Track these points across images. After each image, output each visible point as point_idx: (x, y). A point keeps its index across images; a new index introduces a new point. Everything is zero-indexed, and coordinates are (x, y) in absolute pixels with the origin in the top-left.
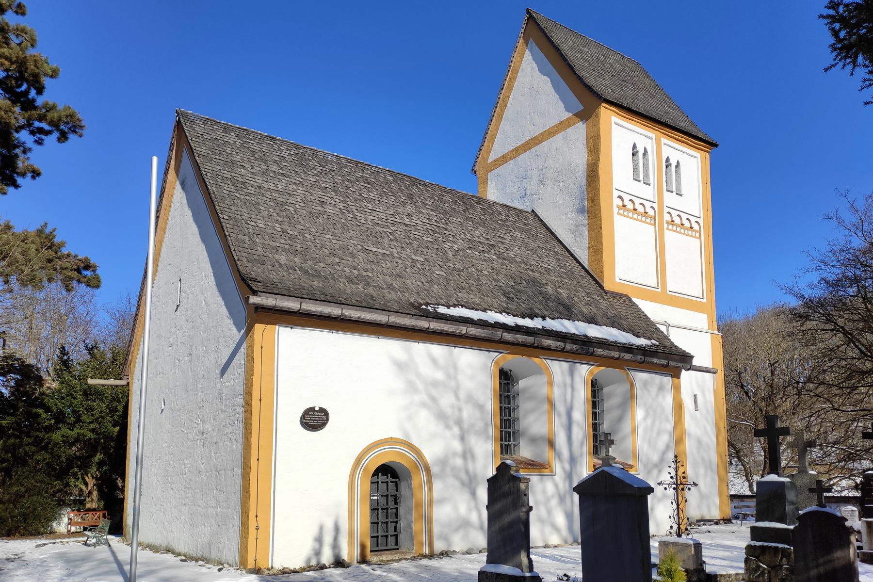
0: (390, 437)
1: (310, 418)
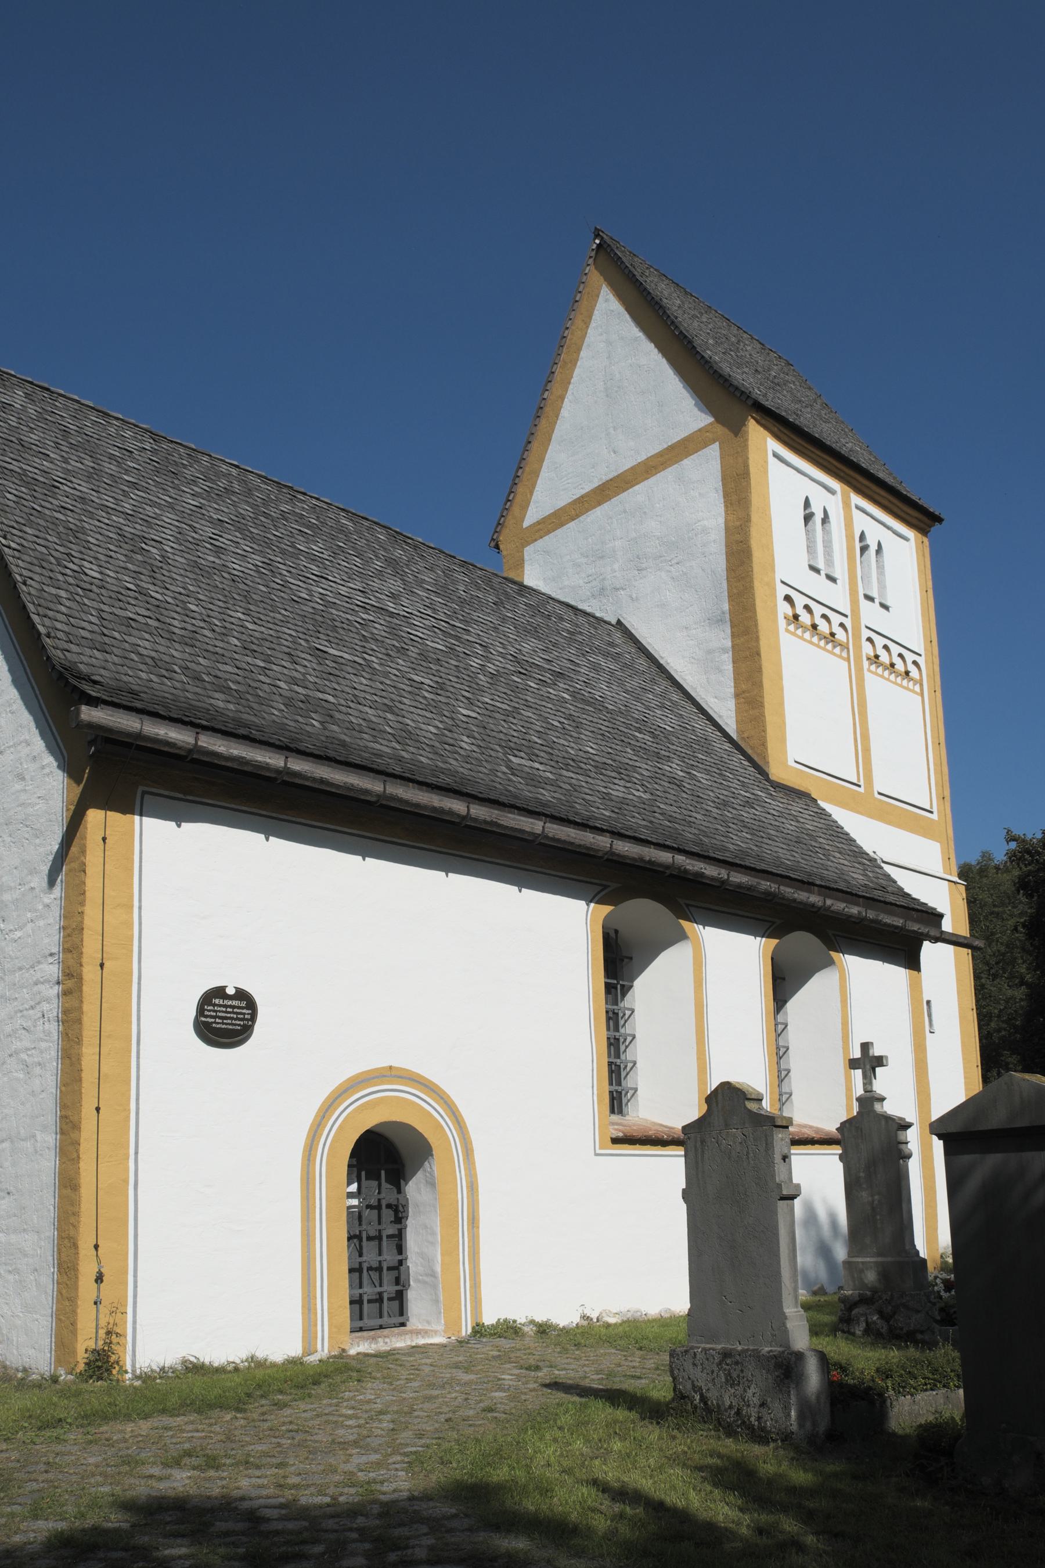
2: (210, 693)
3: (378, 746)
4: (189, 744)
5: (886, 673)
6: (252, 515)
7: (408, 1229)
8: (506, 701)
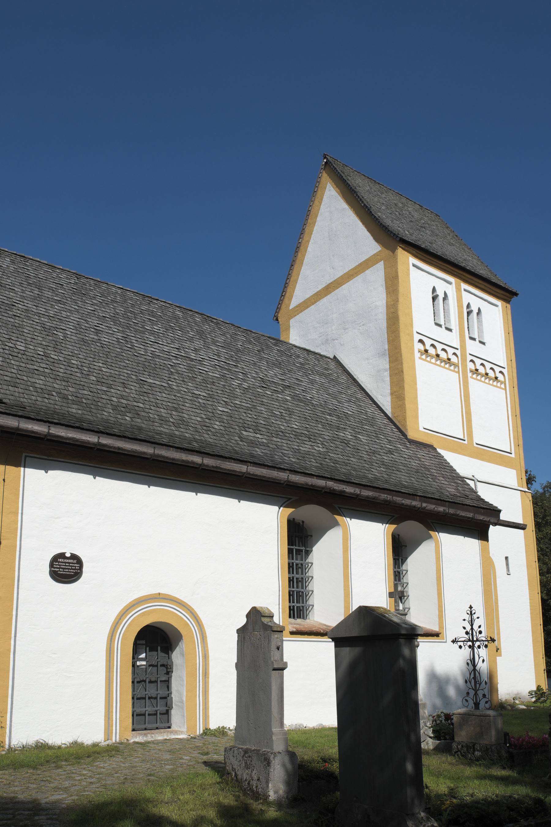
0: (157, 592)
1: (60, 565)
2: (70, 405)
3: (162, 429)
4: (45, 432)
5: (483, 379)
6: (123, 313)
7: (173, 678)
8: (249, 402)
